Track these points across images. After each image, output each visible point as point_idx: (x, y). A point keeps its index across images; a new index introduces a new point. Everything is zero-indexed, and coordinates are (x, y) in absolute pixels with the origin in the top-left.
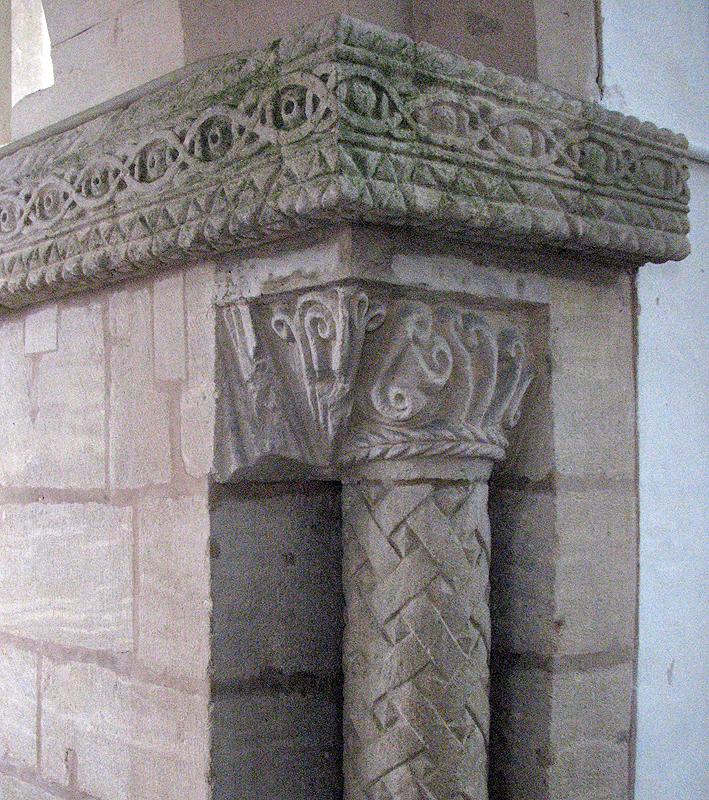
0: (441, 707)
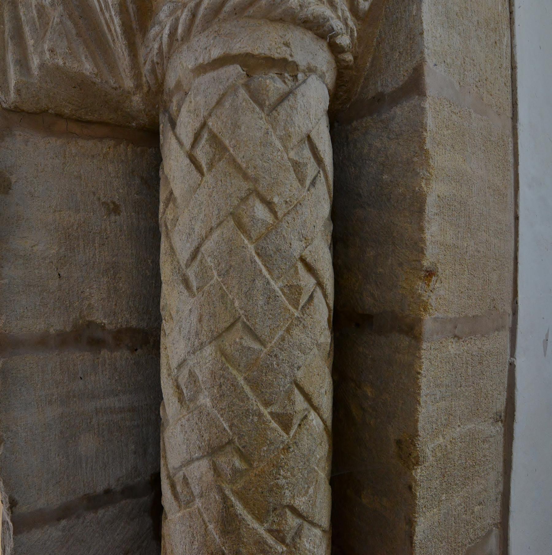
0: (255, 384)
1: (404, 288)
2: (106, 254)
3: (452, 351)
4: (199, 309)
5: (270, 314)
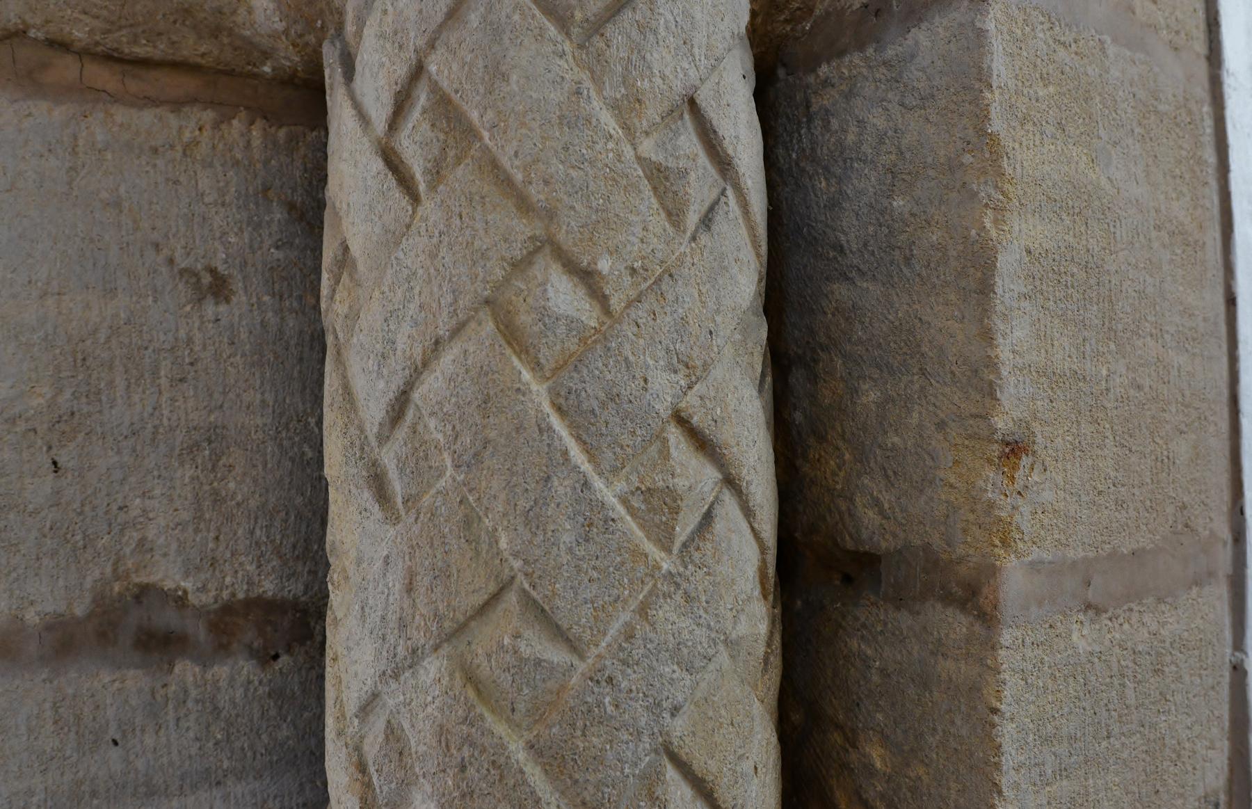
1: (951, 486)
2: (191, 403)
3: (1082, 646)
4: (407, 558)
5: (594, 568)
